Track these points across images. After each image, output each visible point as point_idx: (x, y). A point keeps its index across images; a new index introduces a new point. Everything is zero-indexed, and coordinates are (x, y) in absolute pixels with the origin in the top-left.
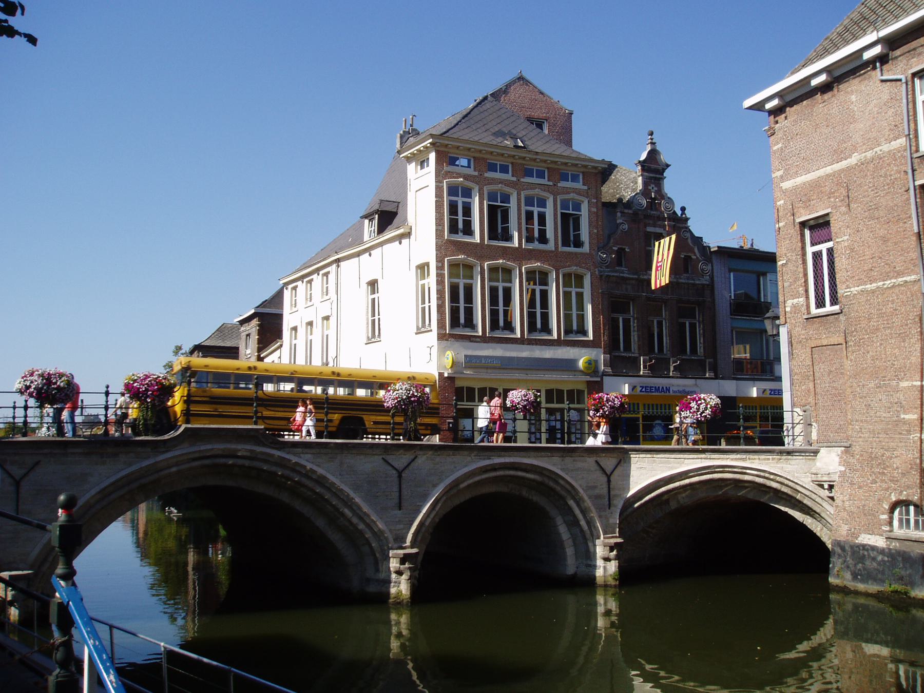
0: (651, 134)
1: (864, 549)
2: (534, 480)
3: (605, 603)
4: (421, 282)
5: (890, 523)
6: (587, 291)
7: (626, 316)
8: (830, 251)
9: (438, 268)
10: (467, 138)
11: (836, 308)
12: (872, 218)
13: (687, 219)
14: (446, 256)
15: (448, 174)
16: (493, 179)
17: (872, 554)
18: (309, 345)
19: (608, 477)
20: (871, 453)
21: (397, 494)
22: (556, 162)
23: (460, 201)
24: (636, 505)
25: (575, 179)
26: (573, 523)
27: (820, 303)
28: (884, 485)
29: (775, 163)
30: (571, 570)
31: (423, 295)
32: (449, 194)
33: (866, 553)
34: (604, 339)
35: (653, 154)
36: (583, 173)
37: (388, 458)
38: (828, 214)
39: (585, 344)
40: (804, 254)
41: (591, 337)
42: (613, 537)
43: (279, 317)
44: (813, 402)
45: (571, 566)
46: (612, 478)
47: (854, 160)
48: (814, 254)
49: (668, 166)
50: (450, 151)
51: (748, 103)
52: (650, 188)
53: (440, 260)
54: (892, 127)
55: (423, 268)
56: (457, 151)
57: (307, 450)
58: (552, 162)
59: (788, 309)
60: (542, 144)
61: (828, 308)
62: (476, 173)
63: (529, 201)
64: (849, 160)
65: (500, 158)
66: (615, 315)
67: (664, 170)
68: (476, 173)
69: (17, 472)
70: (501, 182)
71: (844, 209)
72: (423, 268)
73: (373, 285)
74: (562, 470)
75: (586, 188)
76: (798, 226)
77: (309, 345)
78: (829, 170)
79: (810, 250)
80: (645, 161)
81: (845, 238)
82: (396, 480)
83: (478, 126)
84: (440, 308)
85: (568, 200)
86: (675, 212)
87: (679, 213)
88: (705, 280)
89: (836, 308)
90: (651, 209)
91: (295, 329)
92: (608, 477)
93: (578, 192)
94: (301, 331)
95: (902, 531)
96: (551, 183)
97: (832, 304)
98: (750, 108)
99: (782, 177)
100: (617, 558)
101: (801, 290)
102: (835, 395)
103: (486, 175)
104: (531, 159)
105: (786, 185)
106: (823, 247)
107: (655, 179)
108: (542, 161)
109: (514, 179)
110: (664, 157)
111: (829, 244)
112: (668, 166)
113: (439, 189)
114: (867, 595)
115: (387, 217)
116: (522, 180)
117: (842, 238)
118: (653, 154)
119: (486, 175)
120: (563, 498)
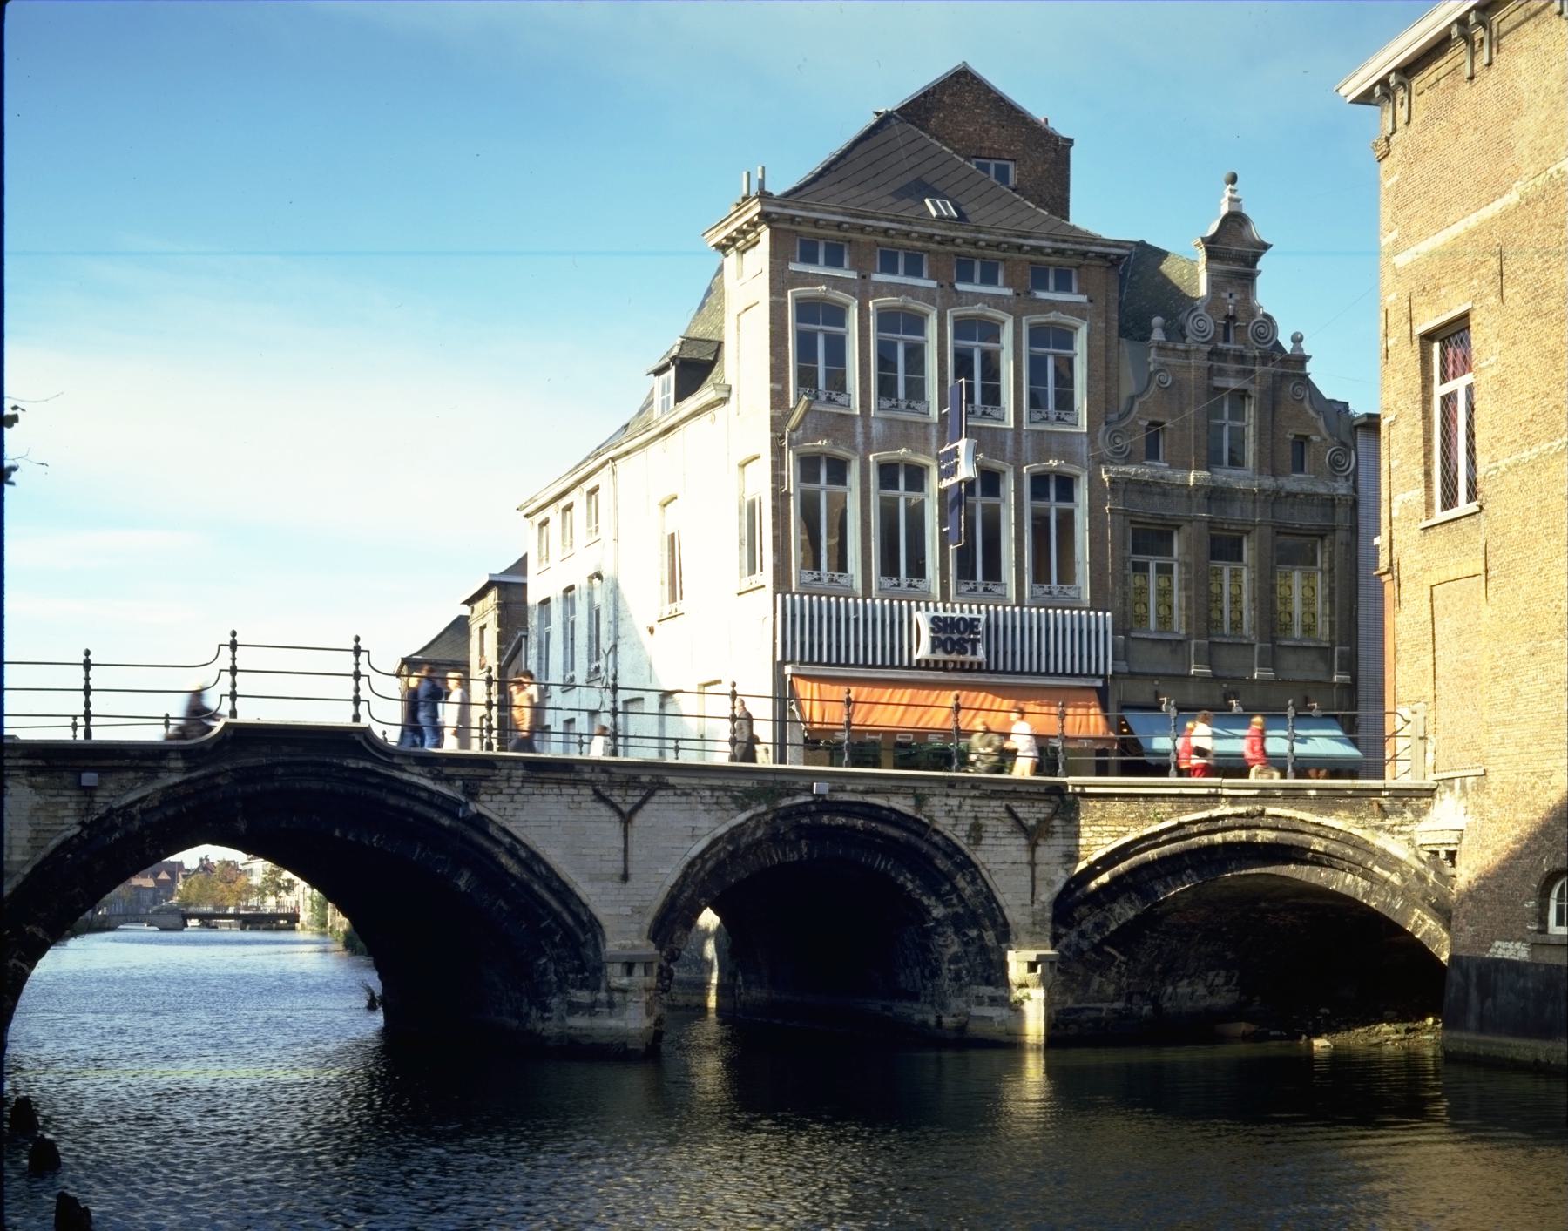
0: (1233, 179)
2: (895, 840)
3: (1034, 1070)
5: (1543, 921)
8: (1470, 389)
11: (1473, 507)
12: (1538, 314)
13: (1303, 360)
20: (1517, 783)
27: (1449, 501)
29: (1386, 213)
35: (1235, 221)
40: (1426, 401)
44: (1430, 698)
49: (1266, 247)
52: (1225, 295)
60: (1007, 218)
63: (964, 327)
64: (1507, 197)
67: (1256, 257)
71: (1493, 300)
76: (1417, 344)
78: (1472, 221)
79: (1439, 390)
81: (1493, 359)
86: (1278, 344)
87: (1288, 346)
89: (1473, 507)
90: (1226, 340)
93: (996, 302)
99: (1396, 243)
100: (1043, 981)
101: (1419, 473)
102: (1466, 677)
103: (877, 277)
105: (1402, 260)
106: (1458, 385)
110: (1260, 229)
111: (1467, 379)
112: (1266, 247)
113: (777, 312)
114: (1537, 1069)
118: (1235, 221)
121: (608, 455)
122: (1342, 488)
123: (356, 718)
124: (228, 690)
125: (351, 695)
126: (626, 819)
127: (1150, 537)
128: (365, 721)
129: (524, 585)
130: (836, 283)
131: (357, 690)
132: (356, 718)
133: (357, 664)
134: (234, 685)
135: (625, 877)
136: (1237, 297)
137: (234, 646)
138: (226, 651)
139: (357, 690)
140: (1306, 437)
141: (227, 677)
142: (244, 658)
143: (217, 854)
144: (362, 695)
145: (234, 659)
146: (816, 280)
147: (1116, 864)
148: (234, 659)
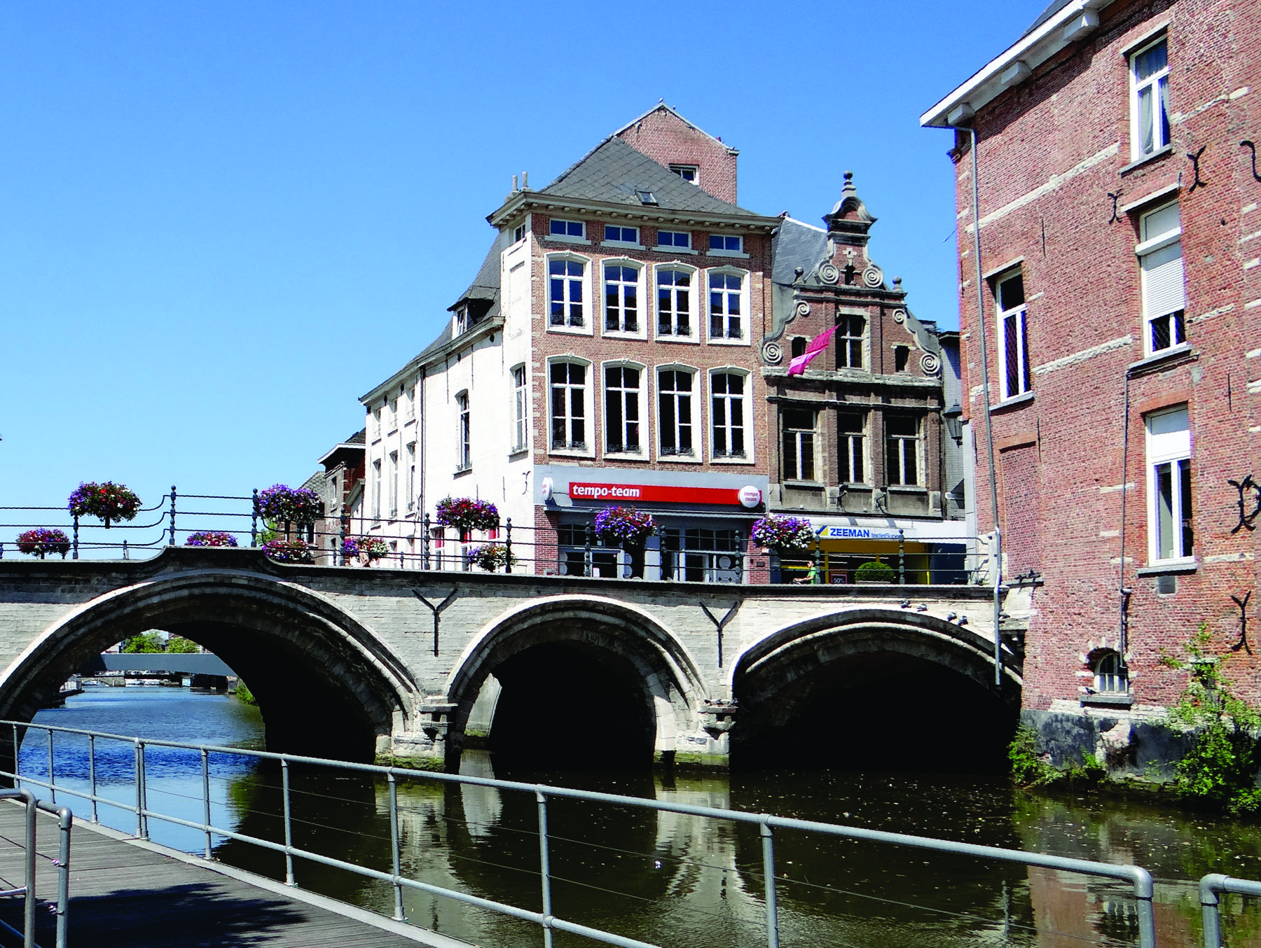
10: (577, 195)
11: (1029, 395)
17: (1068, 725)
22: (702, 223)
24: (749, 670)
25: (732, 244)
27: (1013, 390)
28: (1080, 630)
34: (774, 460)
36: (744, 235)
43: (362, 453)
46: (725, 629)
47: (1053, 183)
49: (873, 220)
50: (554, 213)
51: (925, 119)
52: (846, 252)
54: (1097, 133)
55: (519, 371)
56: (561, 214)
58: (697, 223)
64: (1046, 185)
65: (624, 221)
67: (867, 227)
73: (463, 397)
75: (747, 256)
83: (595, 177)
84: (538, 422)
85: (722, 275)
91: (378, 464)
94: (387, 463)
95: (1104, 694)
96: (696, 253)
98: (929, 125)
100: (731, 732)
104: (666, 221)
106: (1017, 311)
108: (682, 222)
109: (643, 248)
111: (1022, 307)
112: (873, 220)
115: (478, 310)
116: (654, 249)
117: (1035, 294)
121: (424, 369)
123: (254, 544)
124: (168, 526)
125: (250, 528)
126: (720, 627)
127: (795, 416)
131: (255, 526)
134: (173, 523)
135: (436, 652)
136: (855, 253)
137: (173, 496)
138: (168, 500)
141: (168, 517)
142: (180, 504)
143: (153, 631)
147: (355, 636)
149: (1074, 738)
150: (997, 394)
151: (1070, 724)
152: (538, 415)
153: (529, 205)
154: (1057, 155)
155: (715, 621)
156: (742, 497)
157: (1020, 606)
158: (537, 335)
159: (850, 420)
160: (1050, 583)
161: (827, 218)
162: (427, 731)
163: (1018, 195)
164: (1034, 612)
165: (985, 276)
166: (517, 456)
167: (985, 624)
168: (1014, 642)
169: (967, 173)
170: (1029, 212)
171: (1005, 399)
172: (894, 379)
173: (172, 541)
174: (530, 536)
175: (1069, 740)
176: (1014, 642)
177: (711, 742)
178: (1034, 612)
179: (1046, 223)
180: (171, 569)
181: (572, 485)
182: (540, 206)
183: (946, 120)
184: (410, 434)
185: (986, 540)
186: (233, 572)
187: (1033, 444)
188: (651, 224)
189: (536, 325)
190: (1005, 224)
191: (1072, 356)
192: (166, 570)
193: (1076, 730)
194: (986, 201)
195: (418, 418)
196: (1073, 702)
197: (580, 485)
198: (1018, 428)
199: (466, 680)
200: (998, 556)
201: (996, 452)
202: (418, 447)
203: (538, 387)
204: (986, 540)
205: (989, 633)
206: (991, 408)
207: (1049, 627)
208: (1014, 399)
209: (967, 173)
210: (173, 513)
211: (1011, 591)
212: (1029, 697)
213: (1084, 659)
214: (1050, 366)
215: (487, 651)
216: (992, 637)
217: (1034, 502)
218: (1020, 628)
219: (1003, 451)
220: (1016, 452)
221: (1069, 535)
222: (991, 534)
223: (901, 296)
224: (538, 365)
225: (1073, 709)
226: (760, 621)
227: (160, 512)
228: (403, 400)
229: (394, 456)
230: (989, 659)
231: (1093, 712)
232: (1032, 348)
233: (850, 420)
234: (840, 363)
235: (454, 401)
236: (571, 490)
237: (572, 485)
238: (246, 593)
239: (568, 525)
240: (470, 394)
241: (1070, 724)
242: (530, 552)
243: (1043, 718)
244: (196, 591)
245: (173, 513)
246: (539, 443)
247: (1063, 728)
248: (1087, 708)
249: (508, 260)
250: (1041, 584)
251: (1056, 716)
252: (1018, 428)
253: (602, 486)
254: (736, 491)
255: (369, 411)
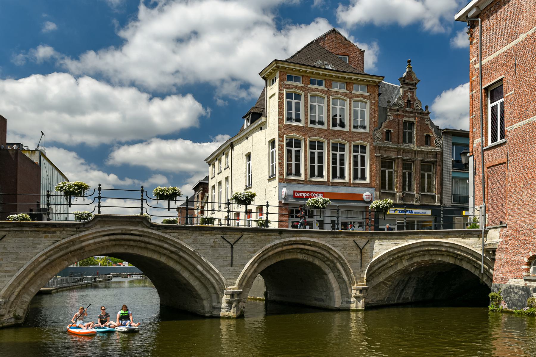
0: (409, 62)
1: (511, 288)
4: (271, 151)
6: (367, 156)
7: (390, 170)
8: (502, 104)
9: (279, 141)
11: (504, 140)
14: (285, 134)
15: (286, 86)
16: (313, 89)
17: (516, 290)
18: (220, 193)
19: (361, 250)
21: (231, 258)
23: (294, 101)
26: (339, 277)
27: (494, 139)
30: (337, 304)
31: (272, 156)
32: (287, 98)
33: (512, 290)
34: (377, 182)
37: (225, 236)
38: (501, 80)
39: (364, 186)
41: (368, 181)
42: (362, 285)
45: (337, 302)
46: (363, 251)
48: (492, 108)
49: (419, 81)
53: (280, 136)
56: (292, 72)
57: (173, 231)
59: (475, 145)
61: (499, 141)
62: (303, 85)
64: (517, 39)
65: (318, 76)
66: (384, 169)
68: (303, 85)
69: (232, 240)
70: (318, 90)
72: (272, 143)
74: (332, 245)
75: (368, 94)
77: (220, 193)
78: (504, 49)
79: (490, 106)
80: (404, 78)
82: (230, 249)
84: (281, 164)
87: (424, 109)
88: (438, 149)
89: (504, 140)
91: (213, 187)
92: (361, 250)
94: (216, 187)
97: (501, 138)
106: (498, 103)
107: (411, 89)
109: (326, 89)
112: (419, 81)
113: (280, 94)
117: (509, 92)
119: (309, 86)
120: (335, 264)
122: (328, 228)
123: (142, 214)
127: (386, 163)
128: (145, 214)
129: (208, 183)
130: (297, 88)
132: (142, 214)
133: (142, 196)
135: (232, 266)
139: (142, 204)
140: (429, 136)
144: (144, 206)
145: (100, 194)
146: (292, 87)
148: (100, 194)
149: (519, 296)
150: (487, 143)
151: (517, 290)
152: (281, 161)
153: (278, 67)
154: (523, 23)
155: (360, 248)
156: (364, 196)
157: (494, 237)
158: (281, 125)
159: (407, 165)
160: (510, 226)
161: (400, 79)
162: (227, 303)
163: (502, 47)
164: (501, 240)
165: (483, 87)
166: (271, 178)
167: (477, 246)
168: (491, 252)
169: (476, 40)
170: (508, 54)
171: (490, 144)
172: (426, 148)
173: (99, 212)
174: (276, 210)
175: (517, 297)
176: (491, 252)
177: (357, 303)
178: (501, 240)
179: (517, 58)
180: (98, 226)
181: (294, 192)
182: (283, 68)
183: (467, 16)
184: (227, 173)
185: (479, 209)
186: (131, 228)
187: (505, 163)
188: (330, 78)
189: (280, 121)
190: (495, 61)
191: (528, 120)
192: (96, 227)
193: (520, 292)
194: (486, 52)
195: (230, 166)
196: (519, 280)
197: (298, 192)
198: (497, 156)
199: (246, 279)
200: (484, 216)
201: (485, 169)
202: (230, 178)
203: (281, 149)
204: (479, 209)
205: (479, 250)
206: (484, 149)
207: (508, 246)
208: (495, 144)
209: (476, 40)
210: (99, 198)
211: (490, 231)
212: (497, 279)
213: (526, 260)
214: (515, 126)
215: (256, 265)
216: (481, 253)
217: (503, 190)
218: (494, 247)
219: (488, 168)
220: (495, 168)
221: (522, 204)
222: (481, 206)
223: (428, 113)
224: (281, 139)
225: (521, 283)
226: (382, 248)
227: (93, 197)
228: (223, 158)
229: (220, 183)
230: (480, 263)
231: (529, 284)
232: (506, 118)
233: (407, 165)
234: (404, 141)
235: (244, 157)
236: (294, 194)
237: (294, 192)
238: (137, 238)
239: (291, 209)
240: (251, 155)
241: (517, 290)
242: (276, 217)
243: (504, 287)
244: (112, 237)
245: (99, 198)
246: (281, 173)
247: (513, 291)
248: (527, 282)
249: (269, 93)
250: (506, 227)
251: (510, 286)
252: (497, 156)
253: (307, 192)
254: (362, 194)
255: (210, 165)
